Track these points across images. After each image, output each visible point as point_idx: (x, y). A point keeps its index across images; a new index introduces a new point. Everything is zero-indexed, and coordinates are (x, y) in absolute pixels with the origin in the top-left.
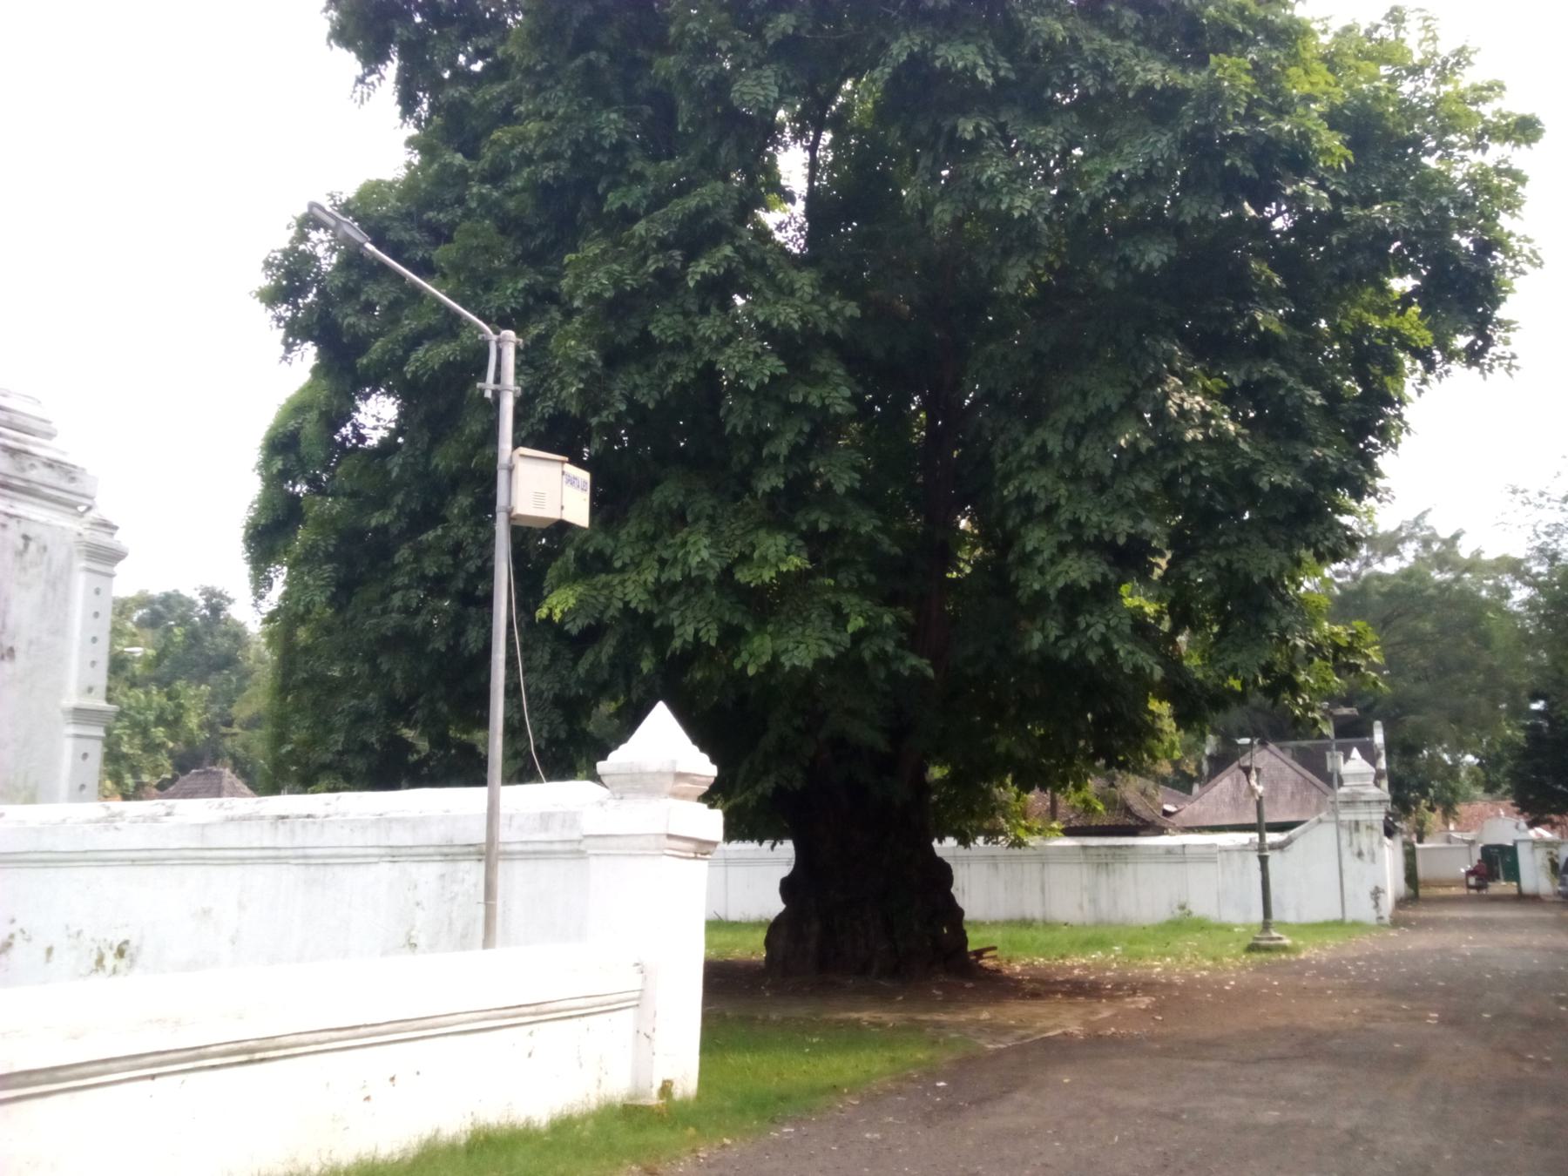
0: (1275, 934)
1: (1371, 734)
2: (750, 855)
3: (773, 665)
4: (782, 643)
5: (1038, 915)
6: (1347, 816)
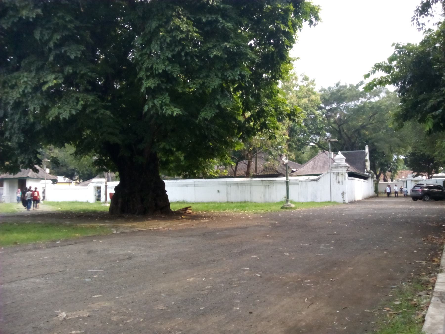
0: (289, 204)
1: (364, 149)
2: (171, 184)
3: (57, 117)
4: (61, 111)
5: (249, 200)
6: (335, 171)
